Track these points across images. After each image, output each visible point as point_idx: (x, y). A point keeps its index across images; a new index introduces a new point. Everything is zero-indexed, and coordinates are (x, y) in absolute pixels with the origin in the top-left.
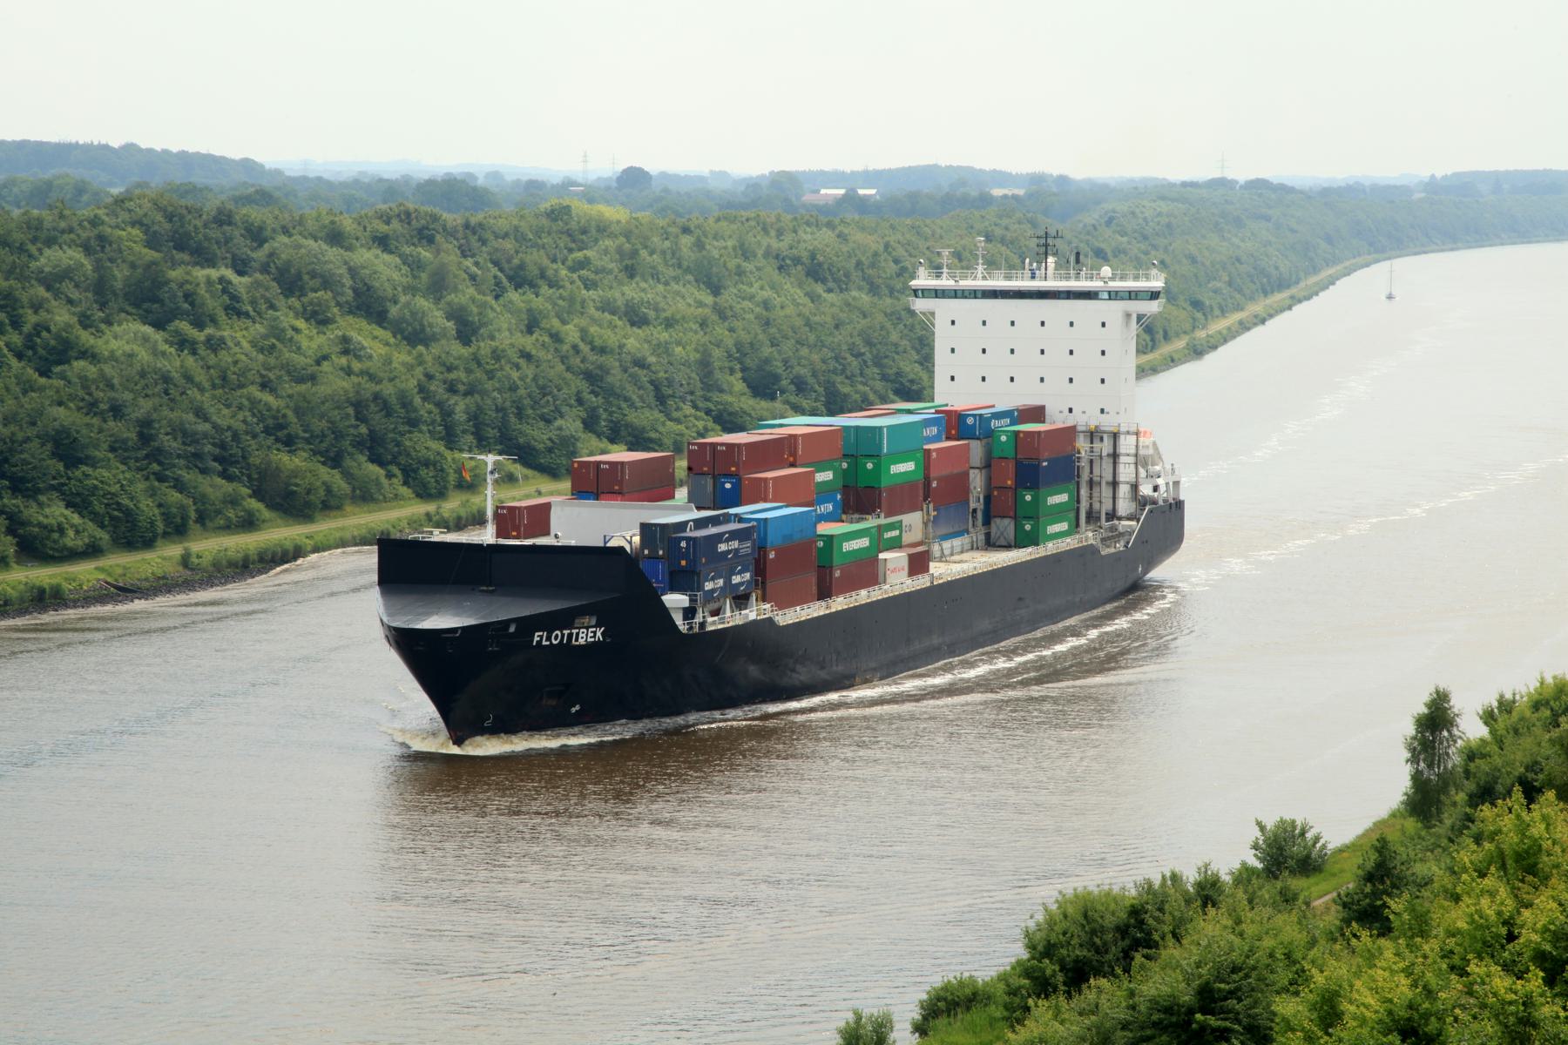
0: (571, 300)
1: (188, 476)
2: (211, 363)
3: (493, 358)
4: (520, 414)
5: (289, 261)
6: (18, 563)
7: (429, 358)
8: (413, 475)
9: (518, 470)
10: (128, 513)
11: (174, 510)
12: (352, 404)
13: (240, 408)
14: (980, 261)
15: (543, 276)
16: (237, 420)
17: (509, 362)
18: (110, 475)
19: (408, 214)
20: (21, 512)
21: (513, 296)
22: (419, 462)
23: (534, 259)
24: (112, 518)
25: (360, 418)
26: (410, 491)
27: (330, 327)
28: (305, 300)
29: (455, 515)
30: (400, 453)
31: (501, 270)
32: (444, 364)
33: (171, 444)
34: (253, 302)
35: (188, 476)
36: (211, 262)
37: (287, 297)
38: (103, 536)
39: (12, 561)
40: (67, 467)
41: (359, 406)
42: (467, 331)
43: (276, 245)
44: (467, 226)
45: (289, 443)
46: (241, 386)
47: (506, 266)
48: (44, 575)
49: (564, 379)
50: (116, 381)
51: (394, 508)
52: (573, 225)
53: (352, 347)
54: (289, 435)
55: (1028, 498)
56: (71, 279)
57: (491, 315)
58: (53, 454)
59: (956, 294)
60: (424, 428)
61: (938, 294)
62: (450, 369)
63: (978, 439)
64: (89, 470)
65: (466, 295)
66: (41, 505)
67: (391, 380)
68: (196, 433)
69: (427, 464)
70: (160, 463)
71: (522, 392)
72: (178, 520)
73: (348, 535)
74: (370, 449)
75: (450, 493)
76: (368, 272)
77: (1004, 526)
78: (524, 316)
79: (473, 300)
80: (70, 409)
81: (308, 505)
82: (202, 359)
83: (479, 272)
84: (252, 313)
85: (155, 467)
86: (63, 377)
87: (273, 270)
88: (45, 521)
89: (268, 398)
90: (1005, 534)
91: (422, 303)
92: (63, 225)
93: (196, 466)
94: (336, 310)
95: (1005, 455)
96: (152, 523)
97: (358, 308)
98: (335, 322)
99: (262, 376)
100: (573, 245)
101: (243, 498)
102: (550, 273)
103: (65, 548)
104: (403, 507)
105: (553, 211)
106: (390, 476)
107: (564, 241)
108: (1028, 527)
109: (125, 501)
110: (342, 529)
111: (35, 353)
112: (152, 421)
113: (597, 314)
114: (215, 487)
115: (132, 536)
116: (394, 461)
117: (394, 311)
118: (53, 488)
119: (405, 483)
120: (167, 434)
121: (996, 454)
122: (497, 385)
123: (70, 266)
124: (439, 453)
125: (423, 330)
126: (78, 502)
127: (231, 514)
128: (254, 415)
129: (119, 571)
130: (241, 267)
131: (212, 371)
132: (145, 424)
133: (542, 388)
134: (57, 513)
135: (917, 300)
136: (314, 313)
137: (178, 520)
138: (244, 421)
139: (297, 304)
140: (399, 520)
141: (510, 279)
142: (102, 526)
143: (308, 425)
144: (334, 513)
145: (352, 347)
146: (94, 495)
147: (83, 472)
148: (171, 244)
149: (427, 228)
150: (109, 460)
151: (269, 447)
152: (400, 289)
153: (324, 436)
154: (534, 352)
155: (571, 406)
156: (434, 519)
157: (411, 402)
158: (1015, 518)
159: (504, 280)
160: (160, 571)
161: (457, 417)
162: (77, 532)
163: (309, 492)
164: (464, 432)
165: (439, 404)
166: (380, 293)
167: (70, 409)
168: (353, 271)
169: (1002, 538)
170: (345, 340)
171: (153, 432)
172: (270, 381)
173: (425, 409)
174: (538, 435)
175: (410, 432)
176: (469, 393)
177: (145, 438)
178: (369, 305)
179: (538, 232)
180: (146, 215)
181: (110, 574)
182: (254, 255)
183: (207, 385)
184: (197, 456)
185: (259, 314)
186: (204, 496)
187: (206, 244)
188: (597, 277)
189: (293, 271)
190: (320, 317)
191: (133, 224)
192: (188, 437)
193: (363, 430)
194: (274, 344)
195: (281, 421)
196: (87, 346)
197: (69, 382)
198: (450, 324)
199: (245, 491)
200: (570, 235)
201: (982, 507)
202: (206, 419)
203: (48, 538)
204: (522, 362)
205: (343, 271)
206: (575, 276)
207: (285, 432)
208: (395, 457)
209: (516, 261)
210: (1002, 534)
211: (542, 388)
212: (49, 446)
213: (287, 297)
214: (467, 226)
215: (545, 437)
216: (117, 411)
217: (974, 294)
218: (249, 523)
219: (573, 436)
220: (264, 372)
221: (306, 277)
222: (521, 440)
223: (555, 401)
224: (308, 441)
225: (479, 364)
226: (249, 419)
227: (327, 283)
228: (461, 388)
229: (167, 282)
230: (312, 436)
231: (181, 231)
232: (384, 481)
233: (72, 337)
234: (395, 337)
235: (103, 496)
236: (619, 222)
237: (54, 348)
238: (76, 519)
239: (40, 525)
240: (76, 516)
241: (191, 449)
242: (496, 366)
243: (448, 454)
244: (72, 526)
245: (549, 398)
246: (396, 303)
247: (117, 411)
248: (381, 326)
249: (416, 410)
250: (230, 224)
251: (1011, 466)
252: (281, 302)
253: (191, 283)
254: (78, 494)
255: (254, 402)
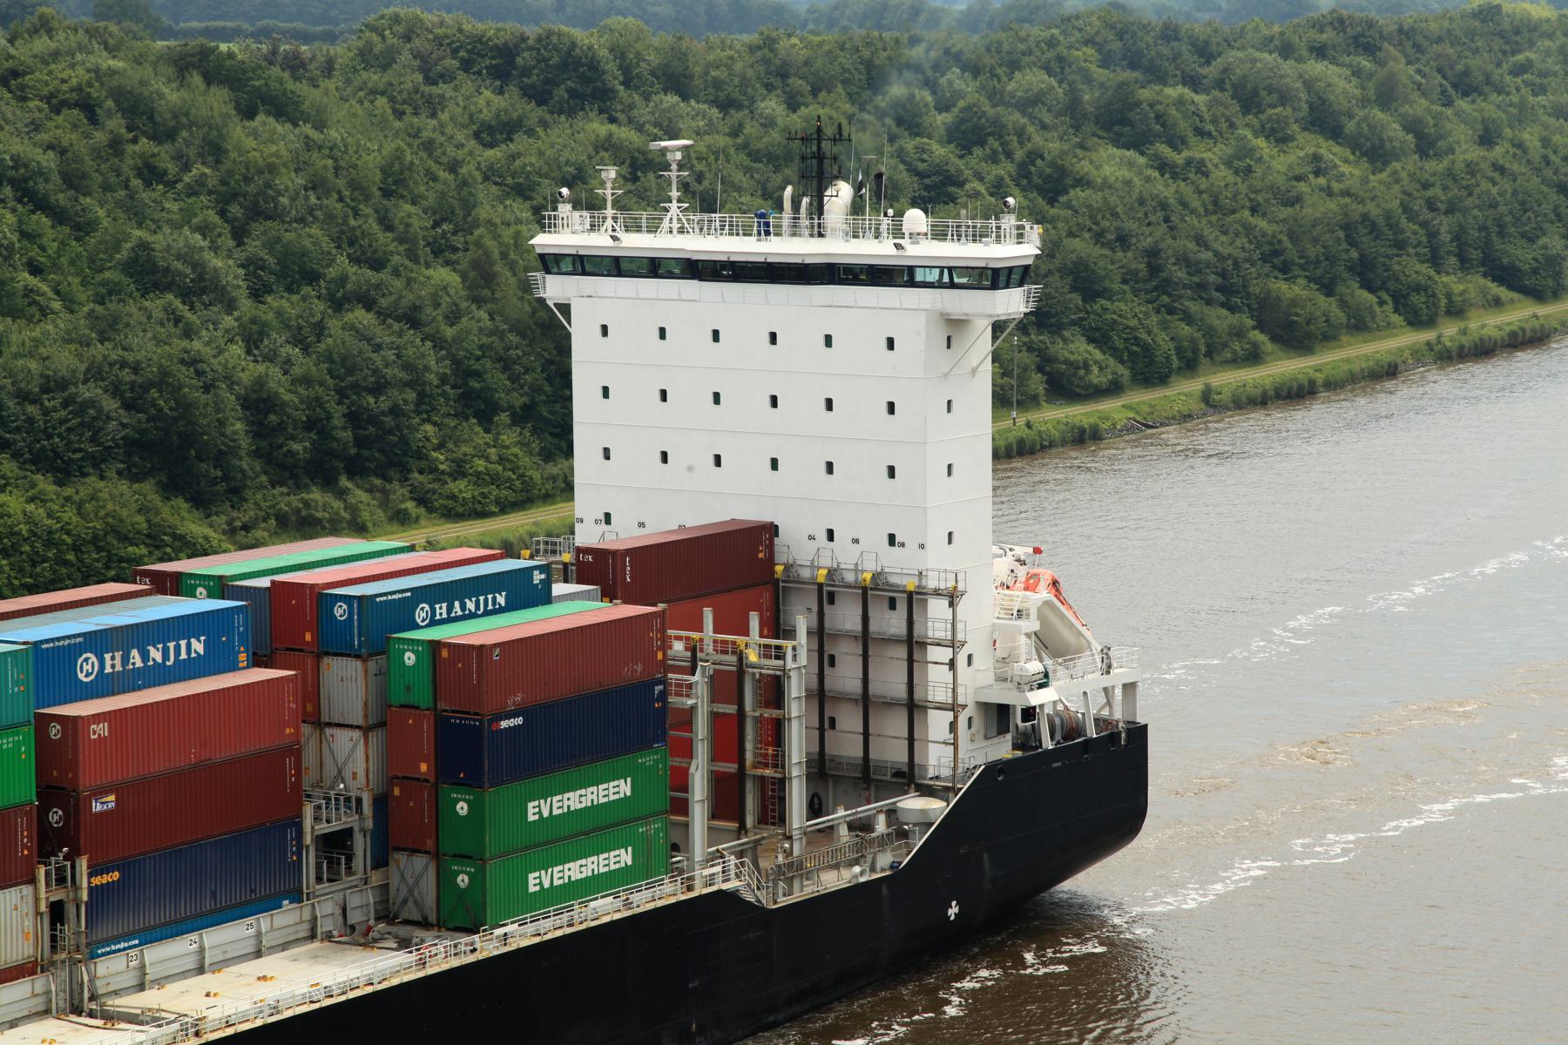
0: (1522, 106)
1: (1194, 307)
2: (1203, 187)
3: (1468, 173)
4: (1502, 234)
5: (1245, 77)
6: (1046, 401)
7: (1404, 174)
8: (1403, 301)
9: (1503, 292)
10: (1146, 348)
11: (1185, 344)
12: (1341, 227)
13: (1237, 235)
14: (675, 194)
15: (1488, 82)
16: (1236, 248)
17: (1484, 176)
18: (1127, 309)
19: (1341, 21)
20: (1047, 348)
21: (1462, 104)
22: (1409, 287)
23: (1478, 64)
24: (1131, 353)
25: (1352, 242)
26: (1401, 318)
27: (1290, 145)
28: (1263, 117)
29: (1457, 344)
30: (1388, 278)
31: (1444, 77)
32: (1419, 181)
33: (1180, 274)
34: (1214, 121)
35: (1194, 307)
36: (1163, 80)
37: (1244, 114)
38: (1124, 371)
39: (1042, 399)
40: (1084, 301)
41: (1347, 227)
42: (1426, 145)
43: (1231, 59)
44: (1401, 31)
45: (1285, 269)
46: (1234, 212)
47: (1449, 73)
48: (1079, 413)
49: (1542, 192)
50: (1119, 210)
51: (1386, 337)
52: (1506, 25)
53: (1323, 166)
54: (1285, 262)
55: (462, 808)
56: (1043, 103)
57: (1449, 126)
58: (1071, 287)
59: (617, 266)
60: (1412, 251)
61: (583, 264)
62: (1426, 186)
63: (358, 656)
64: (1107, 304)
65: (1420, 106)
66: (1065, 340)
67: (1373, 199)
68: (1198, 262)
69: (1418, 289)
70: (1169, 295)
71: (1503, 209)
72: (1189, 354)
73: (1356, 368)
74: (1361, 275)
75: (1440, 319)
76: (1323, 85)
77: (416, 873)
78: (1480, 126)
79: (1429, 110)
80: (1084, 239)
81: (1308, 335)
82: (1193, 183)
83: (1423, 81)
84: (1214, 133)
85: (1165, 299)
86: (1069, 206)
87: (1228, 86)
88: (1072, 358)
89: (1263, 224)
90: (416, 892)
91: (1379, 115)
92: (1022, 47)
93: (1202, 298)
94: (1295, 127)
95: (413, 701)
96: (1168, 358)
97: (1312, 124)
98: (1295, 139)
99: (1251, 200)
100: (1507, 48)
101: (1248, 331)
102: (1495, 78)
103: (1090, 384)
104: (1396, 336)
105: (1481, 12)
106: (1382, 303)
107: (1497, 44)
108: (463, 880)
109: (1143, 336)
110: (1347, 361)
111: (1030, 182)
112: (1160, 251)
113: (1552, 121)
114: (1220, 319)
115: (1150, 372)
116: (1383, 287)
117: (1350, 127)
118: (1074, 323)
119: (1396, 310)
120: (1175, 264)
121: (398, 696)
122: (1477, 202)
123: (1042, 90)
124: (1429, 278)
125: (1382, 146)
126: (1099, 337)
127: (1237, 346)
128: (1250, 242)
129: (1147, 409)
130: (1194, 82)
131: (1204, 196)
132: (1153, 254)
133: (1522, 203)
134: (1082, 349)
135: (549, 278)
136: (1273, 131)
137: (1189, 354)
138: (1243, 249)
139: (1255, 122)
140: (1400, 350)
141: (1455, 86)
142: (1122, 362)
143: (1302, 251)
144: (1332, 344)
145: (1323, 166)
146: (1113, 330)
147: (1102, 306)
148: (1125, 63)
149: (1363, 36)
150: (1124, 293)
151: (1267, 275)
152: (1354, 102)
153: (1318, 262)
154: (1507, 165)
155: (1552, 223)
156: (1436, 348)
157: (1398, 223)
158: (436, 855)
159: (1449, 87)
160: (1186, 409)
161: (1442, 237)
162: (1101, 368)
163: (1309, 322)
164: (1449, 253)
165: (1423, 224)
166: (1335, 107)
167: (1084, 239)
168: (1308, 84)
169: (410, 903)
170: (1316, 158)
171: (1161, 261)
172: (1259, 205)
173: (1410, 228)
174: (1521, 254)
175: (1397, 256)
176: (1450, 211)
177: (1154, 269)
178: (1324, 121)
179: (1471, 34)
180: (1097, 33)
181: (1138, 413)
182: (1205, 71)
183: (1202, 210)
184: (1201, 286)
185: (1221, 133)
186: (1211, 328)
187: (1158, 62)
188: (1545, 81)
189: (1249, 87)
190: (1280, 135)
191: (1086, 43)
192: (1192, 266)
193: (1354, 254)
194: (1249, 166)
195: (1277, 247)
196: (1082, 173)
197: (1076, 212)
198: (1410, 137)
199: (1249, 322)
200: (1503, 37)
201: (369, 824)
202: (1207, 248)
203: (1074, 375)
204: (1497, 176)
205: (1299, 85)
206: (1519, 80)
207: (1282, 258)
208: (1384, 283)
209: (1459, 67)
210: (411, 891)
211: (1522, 203)
212: (1069, 280)
213: (1244, 114)
214: (1401, 31)
215: (1530, 257)
216: (1123, 240)
217: (654, 267)
218: (1254, 357)
219: (1559, 255)
220: (1253, 196)
221: (1263, 93)
222: (1505, 261)
223: (1536, 217)
224: (1303, 267)
225: (1455, 179)
226: (1247, 245)
227: (1284, 98)
228: (1442, 207)
229: (1139, 104)
230: (1307, 262)
231: (1133, 48)
232: (1377, 308)
233: (1067, 164)
234: (1353, 154)
235: (1122, 331)
236: (1548, 20)
237: (1049, 176)
238: (1098, 355)
239: (1066, 362)
240: (1097, 352)
241: (1196, 279)
242: (1473, 181)
243: (1437, 278)
244: (1096, 362)
245: (1529, 214)
246: (1351, 117)
247: (1123, 240)
248: (1338, 144)
249: (1402, 232)
250: (1177, 39)
251: (427, 727)
252: (1239, 121)
253: (1161, 104)
254: (1097, 329)
255: (1249, 229)
